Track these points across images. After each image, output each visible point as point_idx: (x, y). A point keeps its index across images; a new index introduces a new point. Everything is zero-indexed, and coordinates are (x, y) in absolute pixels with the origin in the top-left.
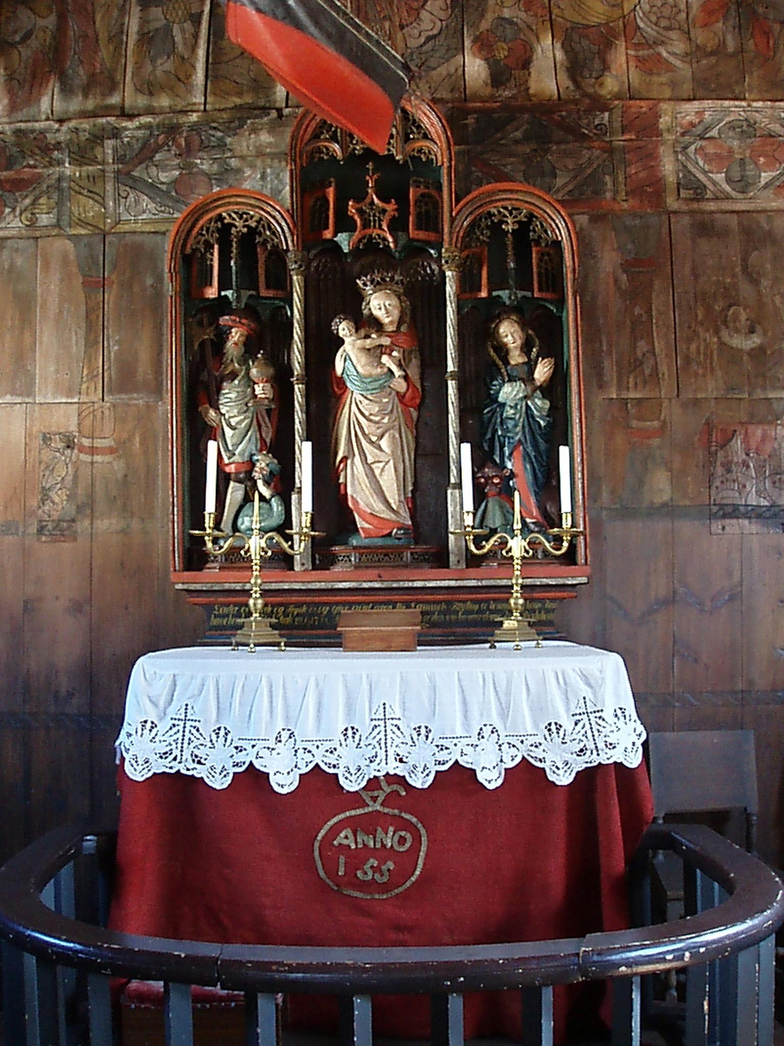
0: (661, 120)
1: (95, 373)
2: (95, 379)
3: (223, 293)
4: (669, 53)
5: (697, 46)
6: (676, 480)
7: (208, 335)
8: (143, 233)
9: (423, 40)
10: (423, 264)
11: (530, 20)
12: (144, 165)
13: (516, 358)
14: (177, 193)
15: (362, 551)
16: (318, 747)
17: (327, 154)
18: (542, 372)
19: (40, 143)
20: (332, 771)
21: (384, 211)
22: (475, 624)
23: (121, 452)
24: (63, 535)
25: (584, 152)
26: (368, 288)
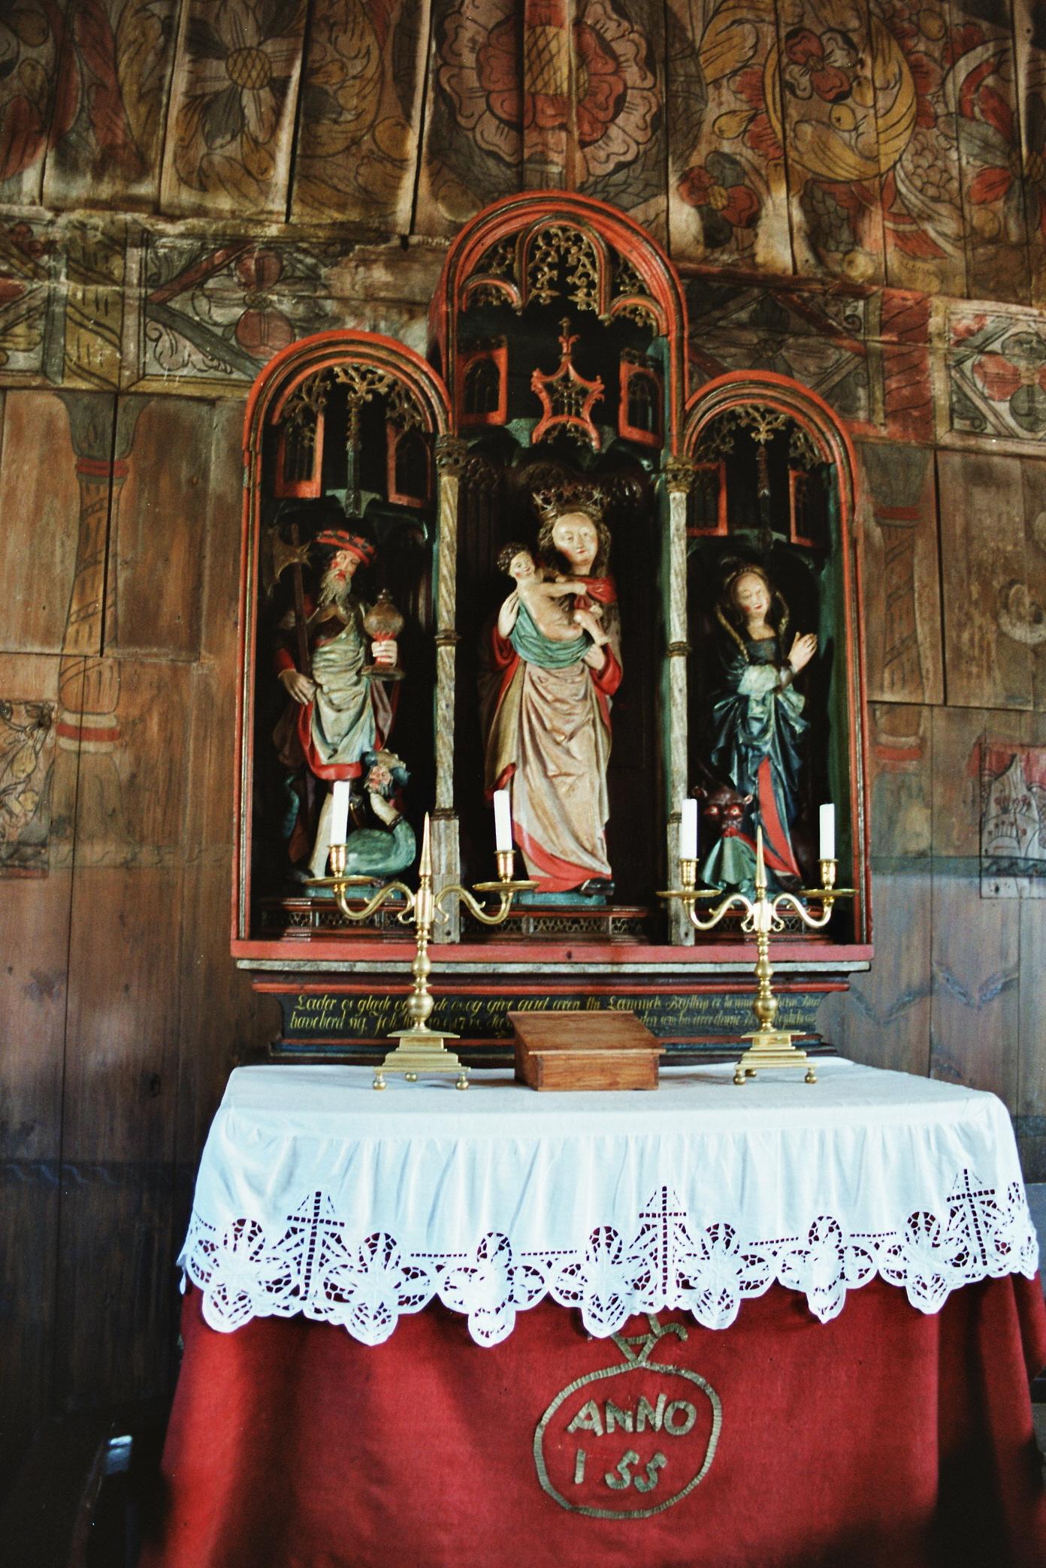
0: (931, 320)
1: (91, 610)
2: (91, 619)
3: (329, 493)
4: (937, 232)
5: (973, 228)
6: (936, 821)
7: (300, 556)
8: (180, 397)
9: (611, 166)
10: (619, 483)
11: (757, 161)
12: (187, 295)
13: (759, 629)
14: (237, 340)
15: (540, 914)
16: (549, 1264)
17: (498, 298)
18: (801, 653)
19: (20, 239)
20: (569, 1304)
21: (584, 392)
22: (704, 1030)
23: (127, 738)
24: (25, 868)
25: (830, 352)
26: (549, 508)
